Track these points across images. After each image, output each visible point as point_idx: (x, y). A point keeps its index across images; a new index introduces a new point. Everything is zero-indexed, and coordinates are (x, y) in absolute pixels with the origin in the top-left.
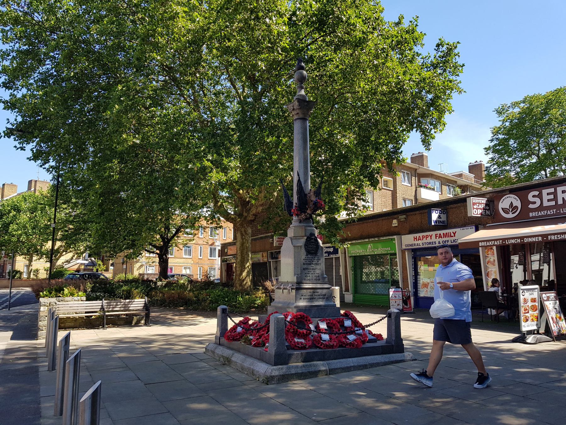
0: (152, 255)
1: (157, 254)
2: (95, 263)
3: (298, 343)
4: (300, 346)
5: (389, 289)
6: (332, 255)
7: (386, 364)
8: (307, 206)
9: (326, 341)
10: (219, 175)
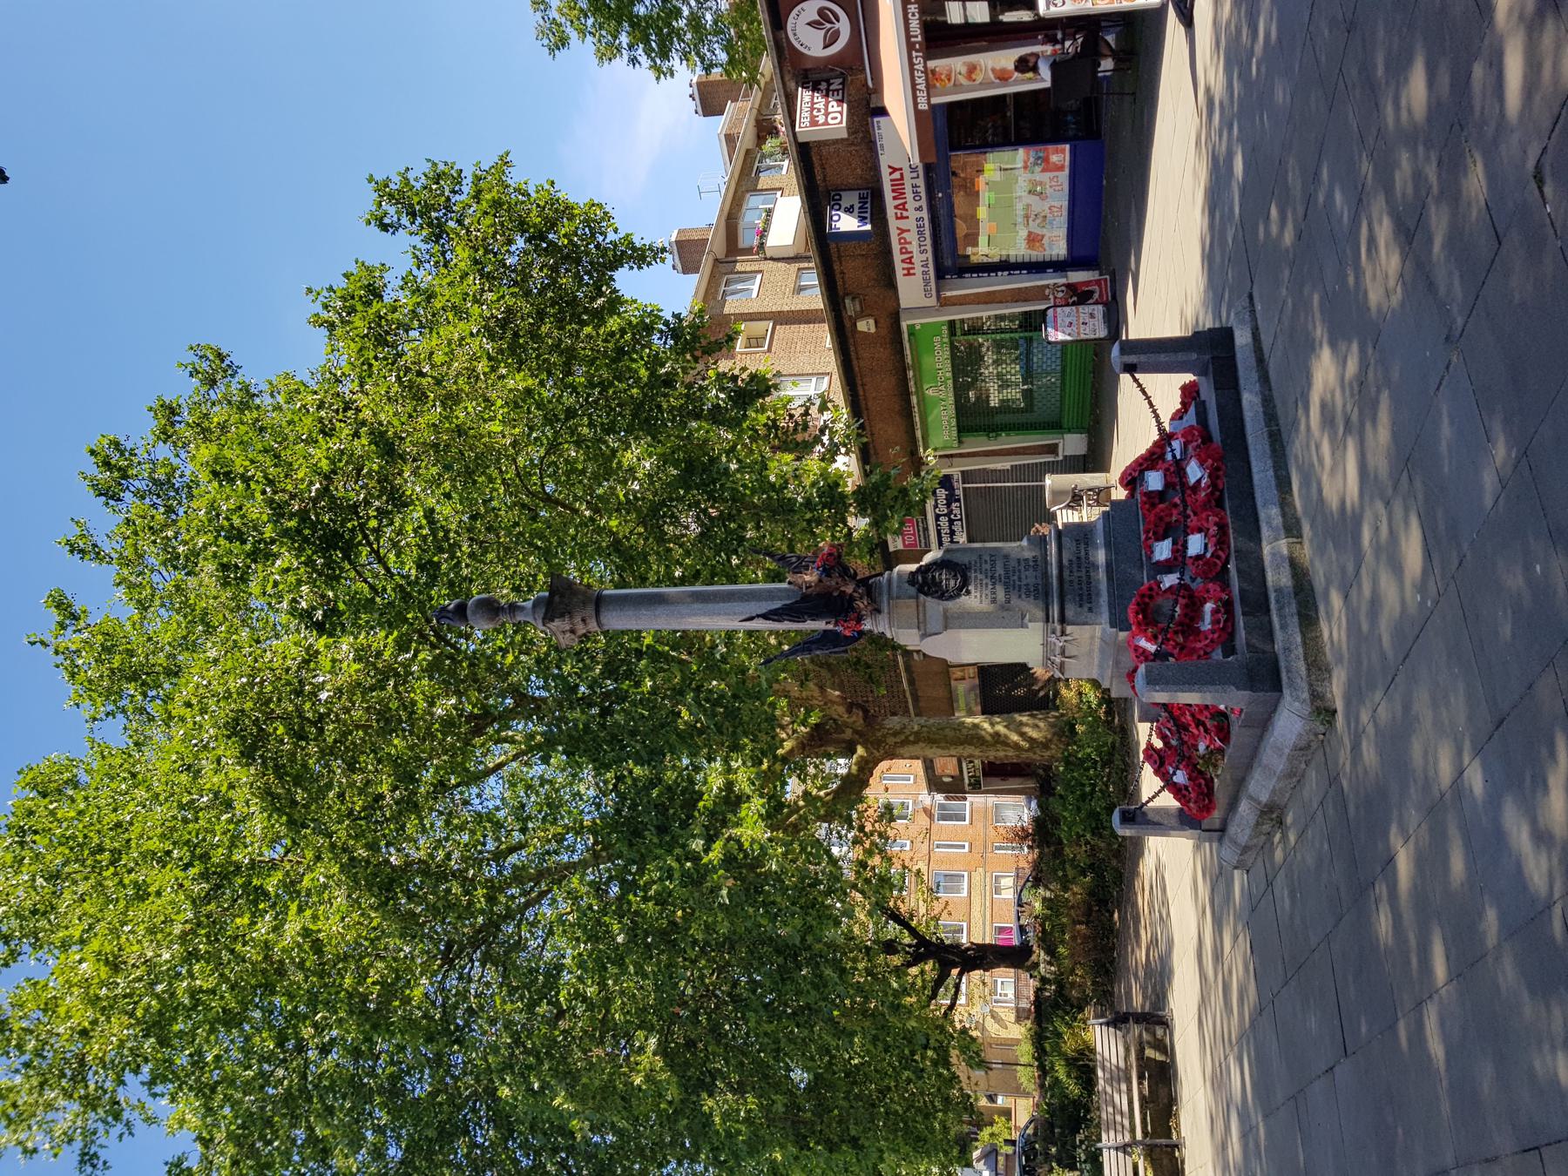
0: (963, 987)
1: (960, 975)
2: (989, 1148)
3: (1215, 622)
4: (1223, 617)
5: (1049, 343)
6: (957, 492)
7: (1264, 379)
8: (835, 594)
9: (1206, 545)
10: (749, 820)
